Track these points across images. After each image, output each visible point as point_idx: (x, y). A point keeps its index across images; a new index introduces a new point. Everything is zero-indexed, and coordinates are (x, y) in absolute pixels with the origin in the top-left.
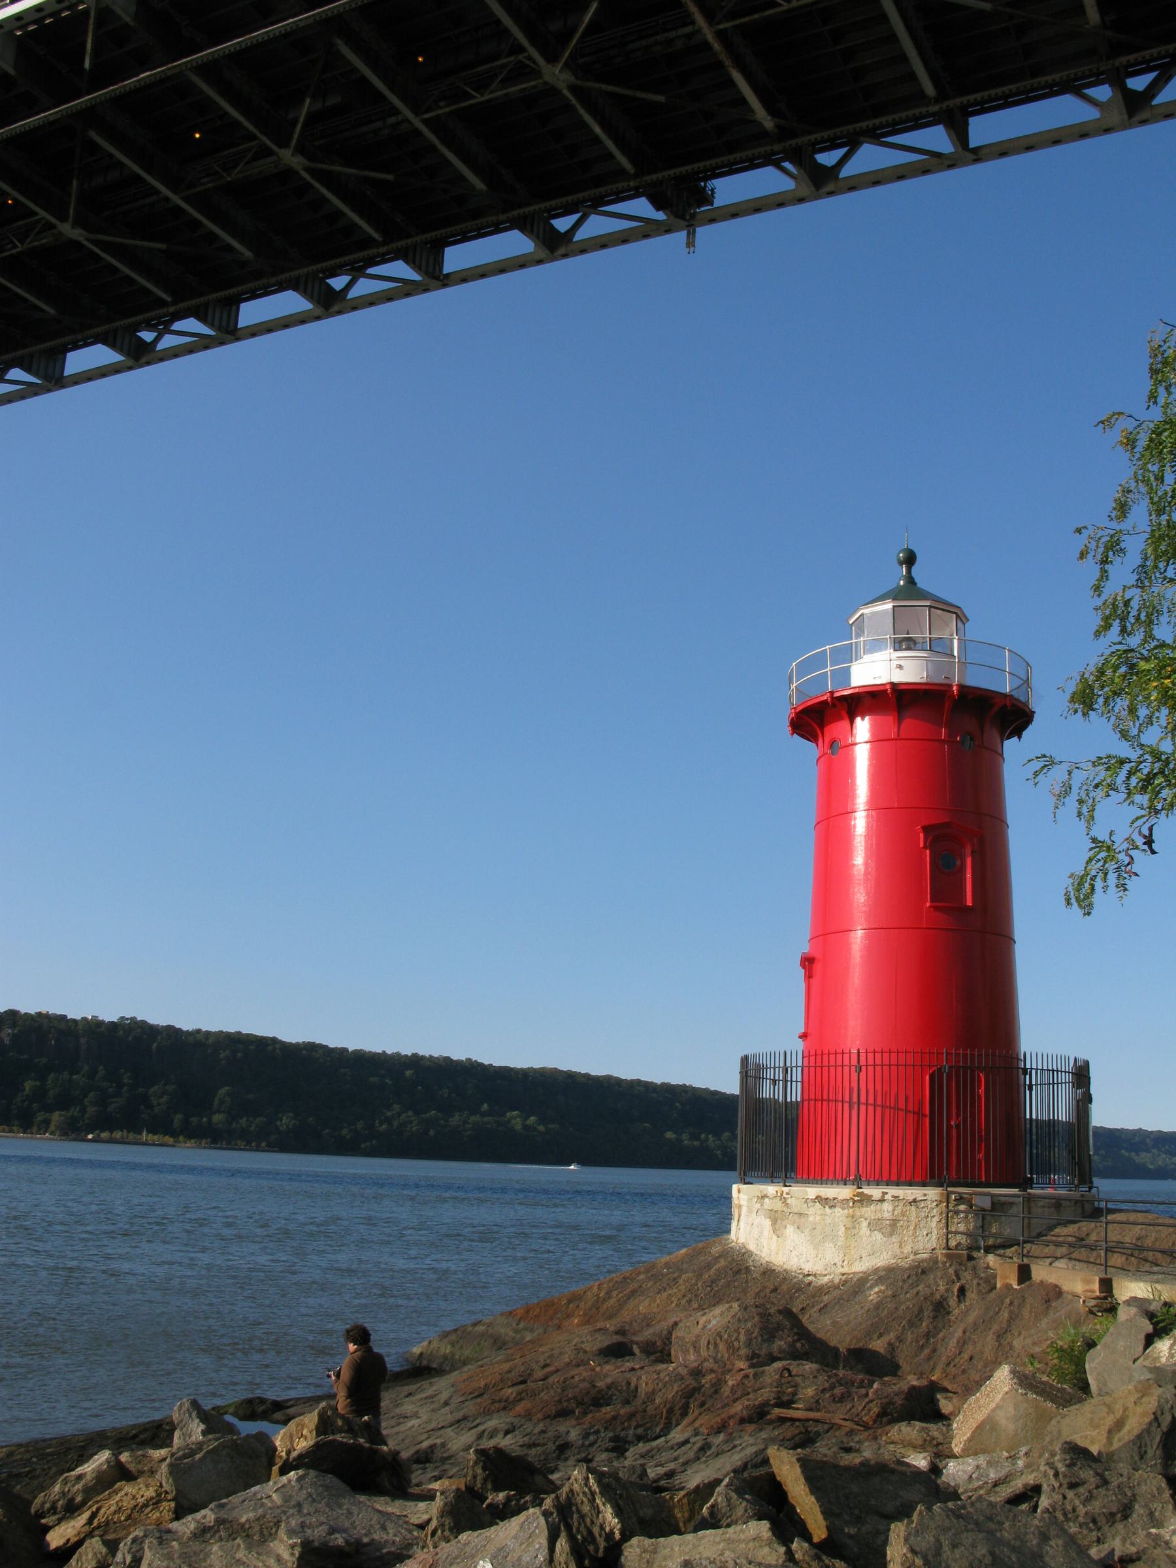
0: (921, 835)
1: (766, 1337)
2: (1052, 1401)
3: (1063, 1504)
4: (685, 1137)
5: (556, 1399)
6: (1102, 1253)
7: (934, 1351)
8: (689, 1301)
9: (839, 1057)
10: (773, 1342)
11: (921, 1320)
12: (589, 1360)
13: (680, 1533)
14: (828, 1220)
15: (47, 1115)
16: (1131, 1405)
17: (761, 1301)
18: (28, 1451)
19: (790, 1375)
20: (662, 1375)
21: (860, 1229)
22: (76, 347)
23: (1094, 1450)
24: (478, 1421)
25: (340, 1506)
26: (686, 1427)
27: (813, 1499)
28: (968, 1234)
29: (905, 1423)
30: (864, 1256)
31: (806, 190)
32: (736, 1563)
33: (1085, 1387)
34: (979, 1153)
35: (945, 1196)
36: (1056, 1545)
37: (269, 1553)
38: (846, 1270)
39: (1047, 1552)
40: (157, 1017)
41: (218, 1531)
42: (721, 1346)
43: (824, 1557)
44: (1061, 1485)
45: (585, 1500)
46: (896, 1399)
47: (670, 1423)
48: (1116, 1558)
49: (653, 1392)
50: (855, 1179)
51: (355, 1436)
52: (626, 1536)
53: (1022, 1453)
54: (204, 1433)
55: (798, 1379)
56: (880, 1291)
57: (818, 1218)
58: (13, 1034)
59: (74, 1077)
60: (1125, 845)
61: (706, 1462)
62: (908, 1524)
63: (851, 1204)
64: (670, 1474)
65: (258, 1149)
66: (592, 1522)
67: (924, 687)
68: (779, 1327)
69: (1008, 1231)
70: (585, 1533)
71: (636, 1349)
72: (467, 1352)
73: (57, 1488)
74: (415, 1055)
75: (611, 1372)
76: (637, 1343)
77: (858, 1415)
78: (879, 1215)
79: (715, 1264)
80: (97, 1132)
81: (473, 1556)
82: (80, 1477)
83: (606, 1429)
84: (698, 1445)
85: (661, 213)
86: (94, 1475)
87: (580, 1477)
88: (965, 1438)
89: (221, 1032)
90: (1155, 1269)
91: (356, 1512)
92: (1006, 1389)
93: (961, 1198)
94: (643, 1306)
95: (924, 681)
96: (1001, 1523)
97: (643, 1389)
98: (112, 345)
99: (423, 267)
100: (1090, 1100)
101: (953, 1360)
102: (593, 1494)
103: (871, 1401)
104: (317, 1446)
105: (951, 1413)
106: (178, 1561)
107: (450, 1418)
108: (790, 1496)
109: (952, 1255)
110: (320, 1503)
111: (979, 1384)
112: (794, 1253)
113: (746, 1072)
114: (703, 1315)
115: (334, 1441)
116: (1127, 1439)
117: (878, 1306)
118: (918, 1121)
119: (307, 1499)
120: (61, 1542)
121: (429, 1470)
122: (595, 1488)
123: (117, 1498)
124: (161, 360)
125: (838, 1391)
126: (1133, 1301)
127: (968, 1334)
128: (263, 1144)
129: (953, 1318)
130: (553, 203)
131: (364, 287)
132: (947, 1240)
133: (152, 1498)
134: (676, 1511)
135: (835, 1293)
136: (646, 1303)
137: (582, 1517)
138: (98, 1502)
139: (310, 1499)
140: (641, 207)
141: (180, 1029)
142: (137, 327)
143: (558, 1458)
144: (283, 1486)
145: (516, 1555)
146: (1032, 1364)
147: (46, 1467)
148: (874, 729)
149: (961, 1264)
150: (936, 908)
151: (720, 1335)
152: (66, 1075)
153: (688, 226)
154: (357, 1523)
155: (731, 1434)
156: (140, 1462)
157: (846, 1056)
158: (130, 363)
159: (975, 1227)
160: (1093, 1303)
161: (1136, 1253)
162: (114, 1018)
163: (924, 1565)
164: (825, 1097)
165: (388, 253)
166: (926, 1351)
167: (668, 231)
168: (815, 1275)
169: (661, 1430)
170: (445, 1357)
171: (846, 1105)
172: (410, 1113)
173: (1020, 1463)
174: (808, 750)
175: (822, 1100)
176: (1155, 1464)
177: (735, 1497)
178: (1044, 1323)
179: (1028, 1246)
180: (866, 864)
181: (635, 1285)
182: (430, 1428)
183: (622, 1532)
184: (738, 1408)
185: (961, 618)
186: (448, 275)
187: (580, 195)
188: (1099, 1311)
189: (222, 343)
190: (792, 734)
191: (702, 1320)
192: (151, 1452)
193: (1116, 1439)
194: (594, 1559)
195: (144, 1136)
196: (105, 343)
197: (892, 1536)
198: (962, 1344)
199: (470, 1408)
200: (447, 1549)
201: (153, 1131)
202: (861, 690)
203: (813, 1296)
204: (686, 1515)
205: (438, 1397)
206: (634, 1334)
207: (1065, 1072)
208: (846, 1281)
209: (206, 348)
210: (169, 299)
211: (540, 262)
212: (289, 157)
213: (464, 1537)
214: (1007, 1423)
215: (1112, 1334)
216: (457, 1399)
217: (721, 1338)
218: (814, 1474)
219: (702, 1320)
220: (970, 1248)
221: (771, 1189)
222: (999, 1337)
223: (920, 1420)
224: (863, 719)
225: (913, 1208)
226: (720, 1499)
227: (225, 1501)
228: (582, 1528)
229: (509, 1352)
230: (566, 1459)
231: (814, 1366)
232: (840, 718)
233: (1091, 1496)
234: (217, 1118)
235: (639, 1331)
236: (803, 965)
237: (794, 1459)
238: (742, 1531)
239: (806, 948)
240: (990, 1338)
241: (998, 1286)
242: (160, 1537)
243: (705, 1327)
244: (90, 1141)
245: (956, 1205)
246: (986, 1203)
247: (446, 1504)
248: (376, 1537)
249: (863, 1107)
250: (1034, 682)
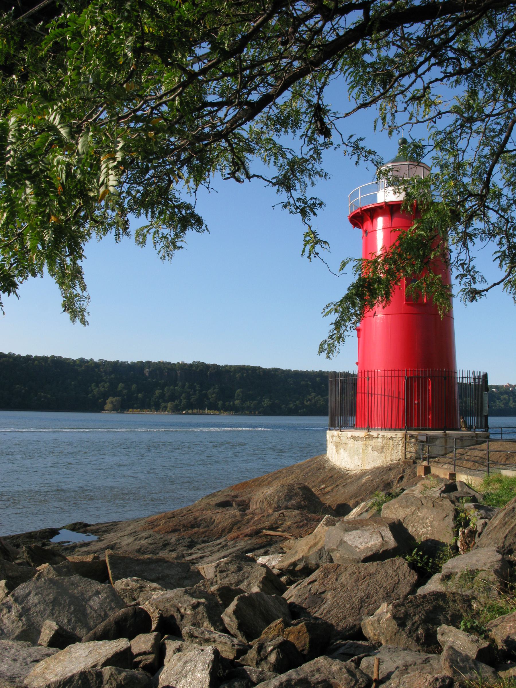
14: (356, 446)
19: (284, 516)
38: (362, 468)
42: (265, 504)
65: (254, 415)
68: (296, 495)
71: (234, 504)
74: (320, 371)
78: (376, 444)
97: (217, 521)
150: (408, 304)
151: (266, 499)
152: (172, 387)
172: (319, 396)
195: (206, 411)
201: (209, 409)
234: (237, 402)
246: (424, 439)
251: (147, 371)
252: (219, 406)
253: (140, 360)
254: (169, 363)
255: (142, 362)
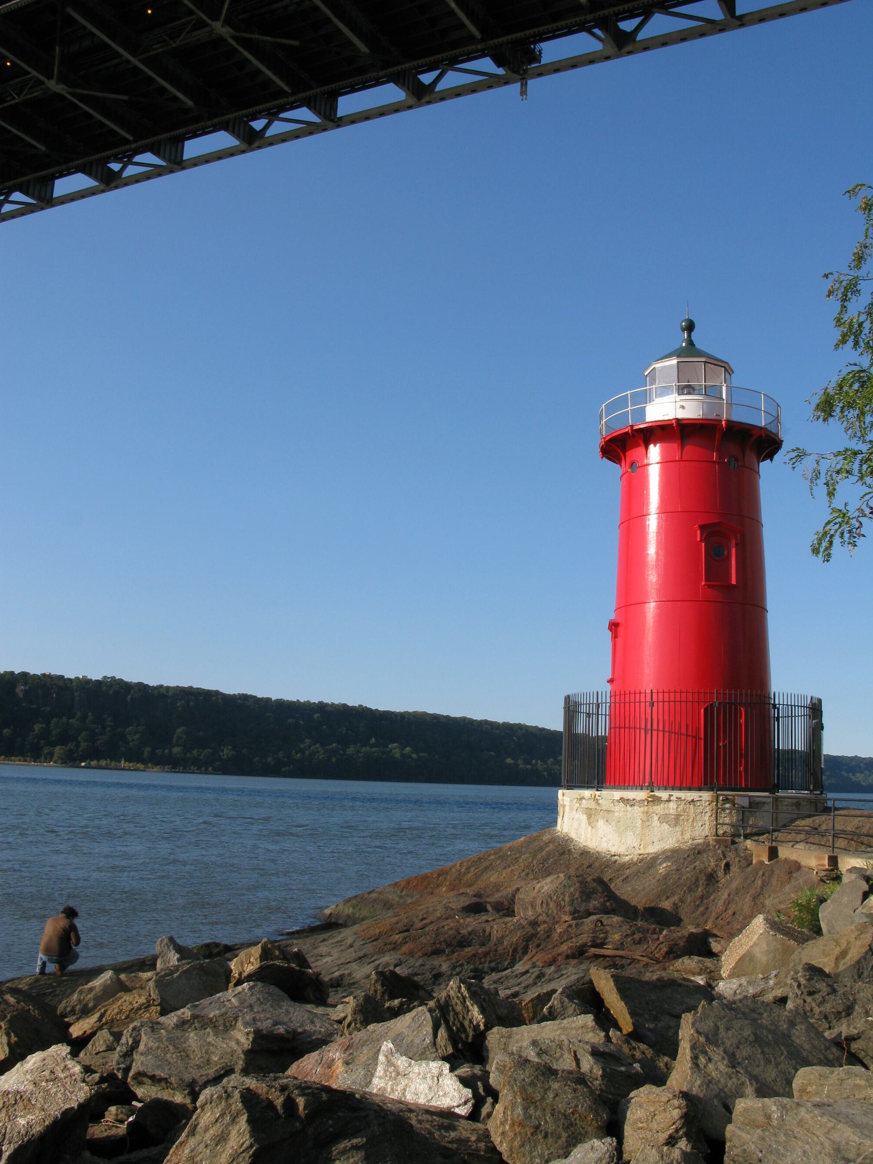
0: (699, 532)
1: (584, 898)
2: (795, 940)
3: (804, 1006)
4: (520, 762)
5: (432, 942)
6: (831, 838)
7: (707, 908)
8: (527, 875)
9: (637, 696)
10: (589, 902)
11: (698, 887)
12: (455, 915)
13: (526, 1025)
14: (629, 815)
15: (51, 749)
16: (852, 940)
17: (580, 872)
18: (49, 979)
19: (602, 925)
20: (509, 925)
21: (652, 822)
22: (62, 176)
23: (827, 970)
24: (375, 958)
25: (281, 1007)
26: (527, 961)
27: (623, 1004)
28: (732, 825)
29: (687, 957)
30: (655, 841)
31: (611, 50)
32: (570, 1042)
33: (818, 931)
34: (740, 766)
35: (715, 798)
36: (800, 1028)
37: (230, 1038)
38: (641, 852)
39: (794, 1034)
40: (131, 677)
41: (194, 1023)
42: (552, 905)
43: (632, 1042)
44: (802, 993)
45: (458, 1002)
46: (679, 941)
47: (515, 959)
48: (843, 1038)
49: (503, 937)
50: (649, 786)
51: (289, 962)
52: (489, 1026)
53: (773, 975)
54: (178, 960)
55: (608, 928)
56: (667, 866)
57: (621, 814)
58: (26, 690)
59: (71, 721)
60: (857, 514)
61: (541, 986)
62: (695, 1014)
63: (646, 804)
64: (515, 995)
65: (206, 772)
66: (464, 1018)
67: (700, 422)
68: (594, 891)
69: (762, 823)
70: (459, 1026)
71: (489, 907)
72: (364, 912)
73: (75, 997)
74: (321, 703)
75: (472, 923)
76: (489, 903)
77: (652, 953)
78: (667, 812)
79: (546, 847)
80: (88, 761)
81: (378, 1040)
82: (91, 989)
83: (468, 963)
84: (535, 974)
85: (501, 69)
86: (101, 988)
87: (455, 986)
88: (731, 967)
89: (178, 687)
90: (869, 849)
91: (292, 1012)
92: (761, 931)
93: (727, 799)
94: (493, 878)
95: (700, 417)
96: (761, 1014)
97: (495, 935)
98: (89, 174)
99: (322, 112)
100: (822, 728)
101: (721, 915)
102: (464, 998)
103: (662, 943)
104: (261, 968)
105: (720, 952)
106: (166, 1043)
107: (354, 956)
108: (605, 1002)
109: (720, 840)
110: (266, 1005)
111: (740, 931)
112: (604, 840)
113: (569, 707)
114: (538, 883)
115: (275, 964)
116: (849, 964)
117: (666, 877)
118: (696, 744)
119: (256, 1002)
120: (80, 1033)
121: (340, 992)
122: (466, 994)
123: (119, 1003)
124: (126, 185)
125: (637, 936)
126: (853, 870)
127: (731, 896)
128: (210, 769)
129: (721, 885)
130: (420, 62)
131: (277, 128)
132: (717, 829)
133: (143, 1004)
134: (523, 1012)
135: (635, 868)
136: (496, 875)
137: (456, 1014)
138: (105, 1006)
139: (259, 1002)
140: (486, 65)
141: (147, 685)
142: (108, 160)
143: (434, 984)
144: (239, 993)
145: (410, 1039)
146: (778, 917)
147: (63, 989)
148: (663, 454)
149: (726, 847)
150: (709, 586)
152: (64, 720)
153: (521, 79)
154: (293, 1018)
155: (559, 966)
156: (133, 981)
157: (643, 695)
158: (103, 187)
159: (737, 820)
160: (823, 873)
161: (855, 838)
162: (99, 677)
163: (706, 1041)
164: (627, 725)
165: (295, 102)
166: (701, 909)
167: (506, 83)
168: (619, 856)
169: (508, 964)
170: (348, 916)
171: (643, 732)
172: (318, 745)
173: (771, 982)
174: (613, 470)
175: (625, 728)
176: (869, 981)
177: (567, 1000)
178: (787, 888)
179: (776, 834)
180: (657, 553)
181: (487, 863)
182: (340, 962)
183: (485, 1025)
184: (564, 948)
185: (728, 370)
186: (341, 118)
187: (440, 56)
188: (827, 880)
189: (172, 172)
190: (602, 458)
191: (538, 886)
192: (141, 974)
193: (841, 964)
194: (465, 1043)
196: (84, 172)
197: (683, 1022)
198: (728, 903)
199: (369, 948)
200: (360, 1036)
201: (129, 760)
202: (654, 424)
203: (618, 871)
204: (531, 1015)
205: (345, 941)
206: (488, 897)
207: (801, 706)
208: (642, 860)
209: (160, 175)
210: (131, 138)
211: (410, 107)
212: (220, 28)
213: (371, 1027)
214: (761, 955)
215: (838, 892)
216: (358, 943)
217: (551, 899)
218: (624, 987)
219: (538, 886)
220: (733, 835)
221: (587, 793)
222: (755, 898)
223: (699, 956)
224: (655, 446)
225: (692, 806)
226: (556, 1003)
227: (197, 1003)
228: (456, 1022)
229: (395, 910)
230: (440, 984)
231: (620, 919)
232: (637, 445)
233: (824, 1001)
234: (176, 750)
235: (491, 895)
236: (610, 629)
237: (609, 976)
238: (573, 1022)
239: (612, 616)
240: (748, 899)
241: (754, 862)
242: (152, 1027)
243: (539, 891)
244: (83, 767)
245: (723, 804)
246: (745, 802)
247: (357, 1005)
248: (307, 1028)
249: (655, 733)
250: (783, 419)
251: (20, 689)
252: (146, 755)
253: (9, 670)
254: (61, 677)
255: (12, 673)
